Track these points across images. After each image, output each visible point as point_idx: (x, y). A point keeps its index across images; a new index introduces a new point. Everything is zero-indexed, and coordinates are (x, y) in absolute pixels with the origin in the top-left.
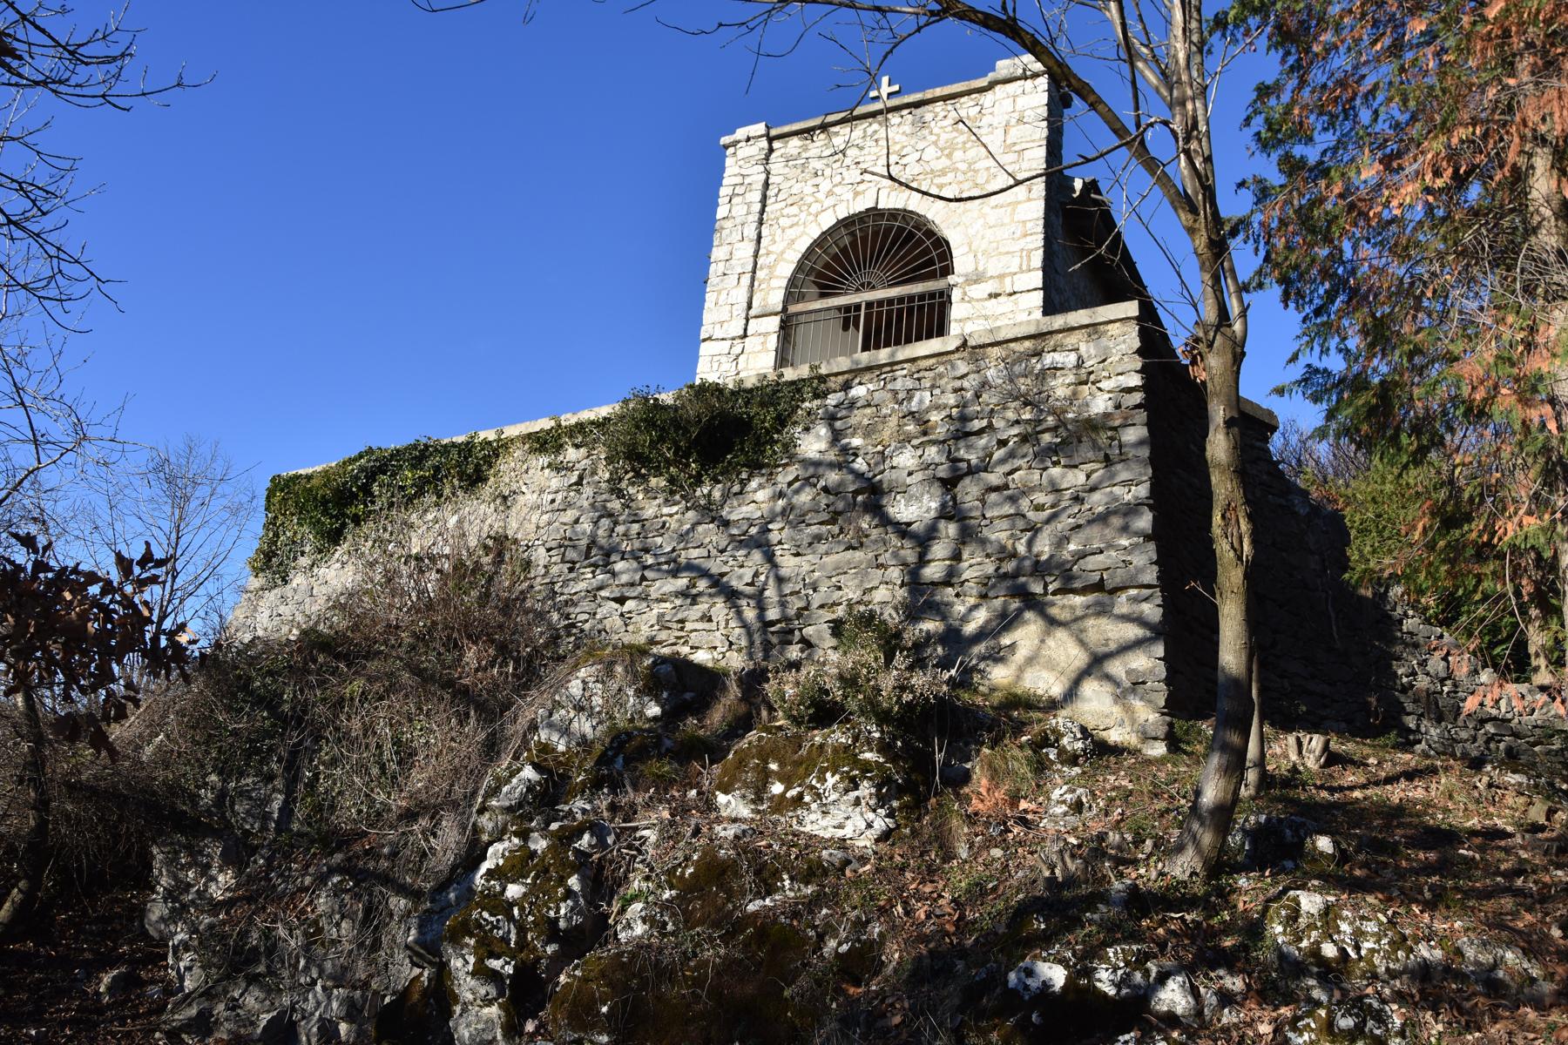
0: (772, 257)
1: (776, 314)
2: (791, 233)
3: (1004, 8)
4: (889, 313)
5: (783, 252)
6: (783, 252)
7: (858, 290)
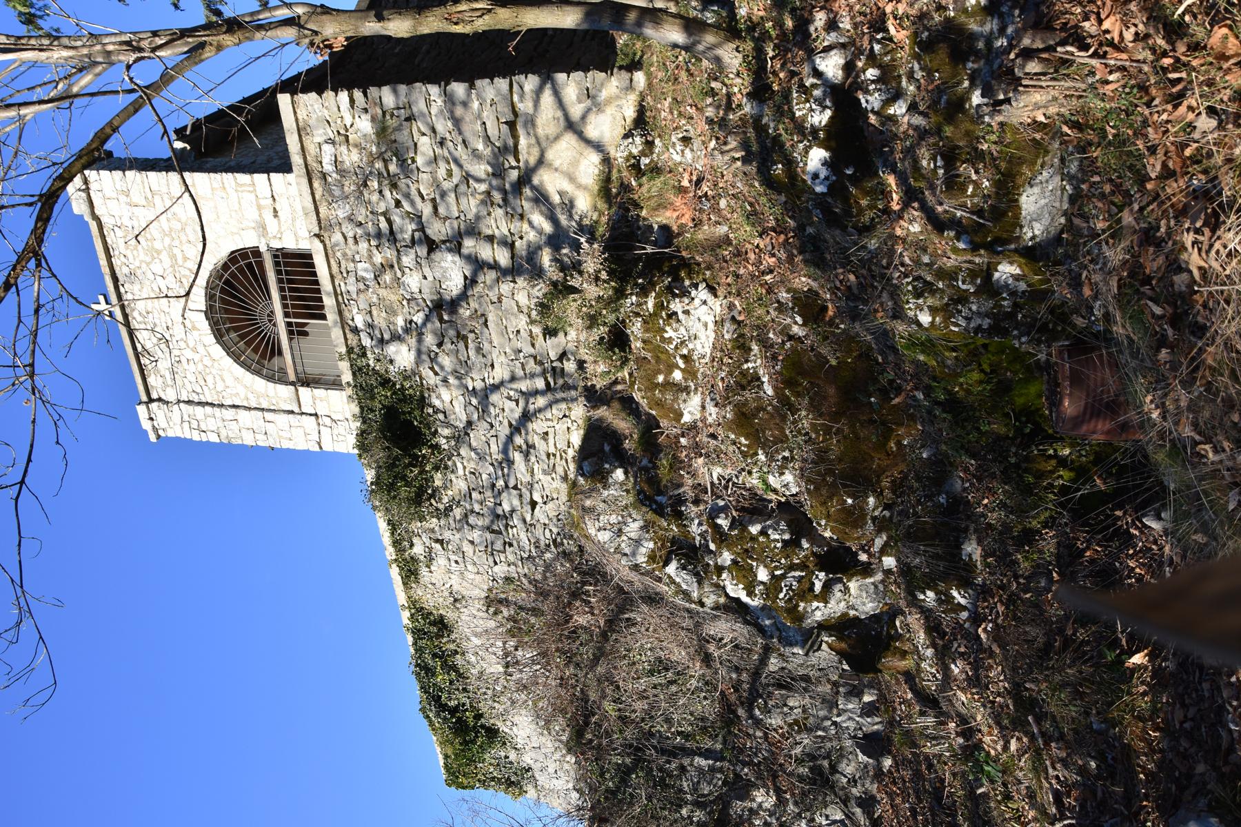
1: (297, 390)
5: (246, 387)
7: (274, 325)
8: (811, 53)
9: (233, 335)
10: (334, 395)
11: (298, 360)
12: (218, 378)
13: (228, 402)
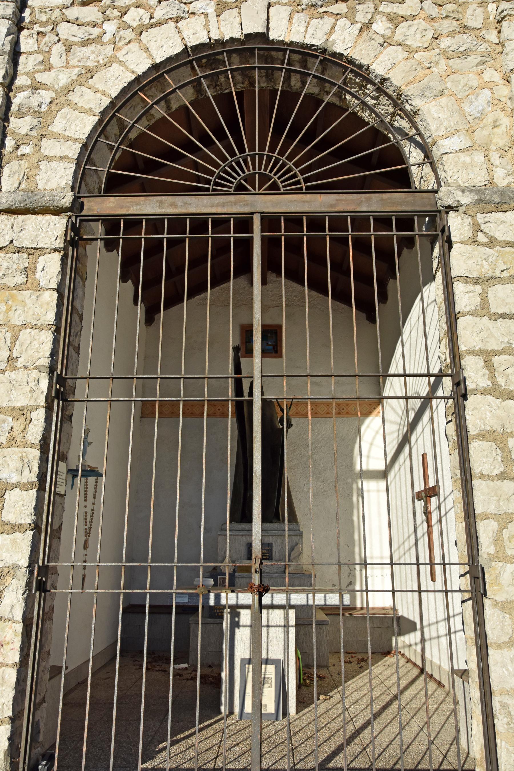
0: (46, 96)
1: (57, 212)
2: (88, 55)
3: (2, 68)
4: (199, 246)
5: (69, 90)
6: (69, 90)
7: (240, 188)
8: (355, 608)
9: (184, 98)
10: (18, 624)
11: (423, 529)
12: (96, 31)
13: (27, 42)
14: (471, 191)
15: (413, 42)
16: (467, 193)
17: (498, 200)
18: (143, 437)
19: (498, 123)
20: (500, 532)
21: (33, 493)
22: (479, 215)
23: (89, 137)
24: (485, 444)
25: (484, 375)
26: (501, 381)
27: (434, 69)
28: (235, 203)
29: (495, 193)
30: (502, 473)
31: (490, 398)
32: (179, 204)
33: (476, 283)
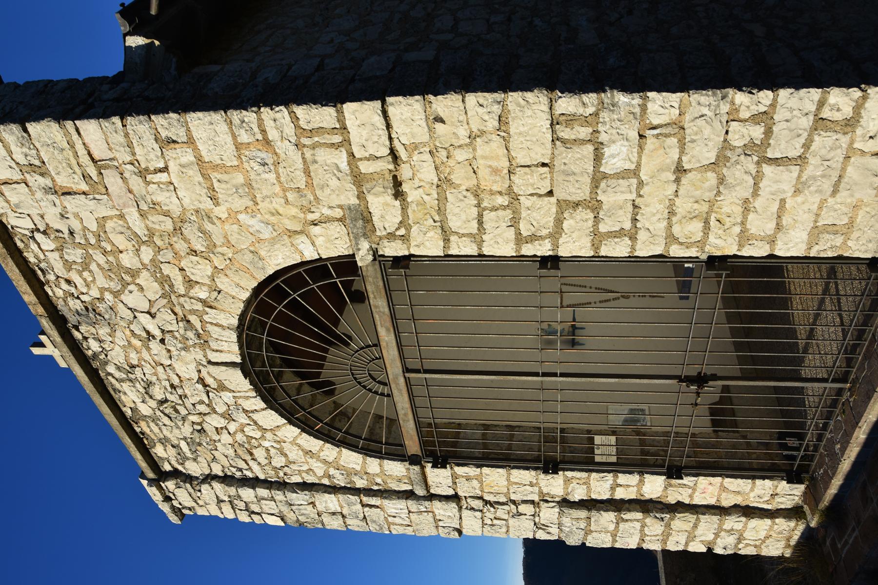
14: (357, 244)
15: (209, 271)
16: (360, 247)
17: (361, 222)
18: (582, 431)
19: (274, 211)
20: (681, 244)
21: (619, 475)
22: (378, 233)
23: (360, 453)
24: (603, 248)
25: (540, 245)
26: (544, 232)
27: (230, 255)
28: (397, 384)
29: (355, 226)
30: (630, 238)
31: (561, 241)
32: (403, 412)
33: (449, 240)
